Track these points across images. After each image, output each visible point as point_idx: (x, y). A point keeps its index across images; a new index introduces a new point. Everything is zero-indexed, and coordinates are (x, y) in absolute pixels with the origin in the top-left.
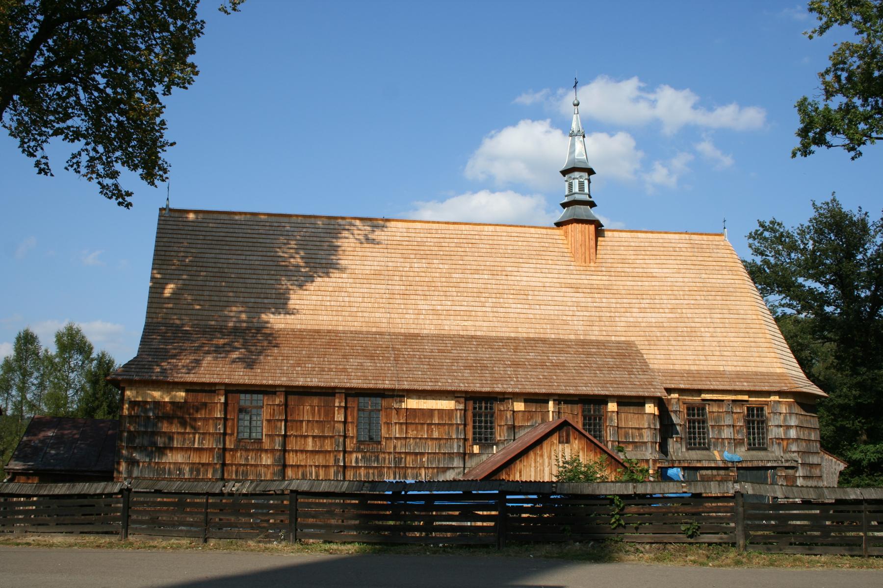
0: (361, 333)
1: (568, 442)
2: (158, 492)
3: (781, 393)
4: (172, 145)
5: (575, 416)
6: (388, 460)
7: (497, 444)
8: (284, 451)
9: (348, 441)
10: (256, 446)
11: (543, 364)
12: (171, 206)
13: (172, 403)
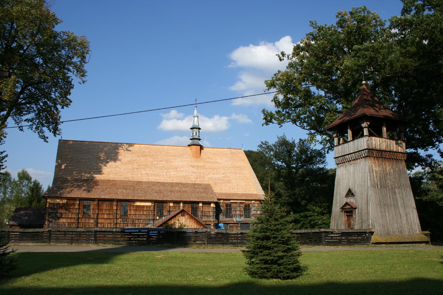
0: (123, 181)
1: (184, 216)
2: (59, 231)
3: (255, 200)
5: (188, 208)
6: (130, 221)
7: (164, 216)
8: (97, 218)
9: (117, 215)
10: (89, 217)
13: (63, 203)
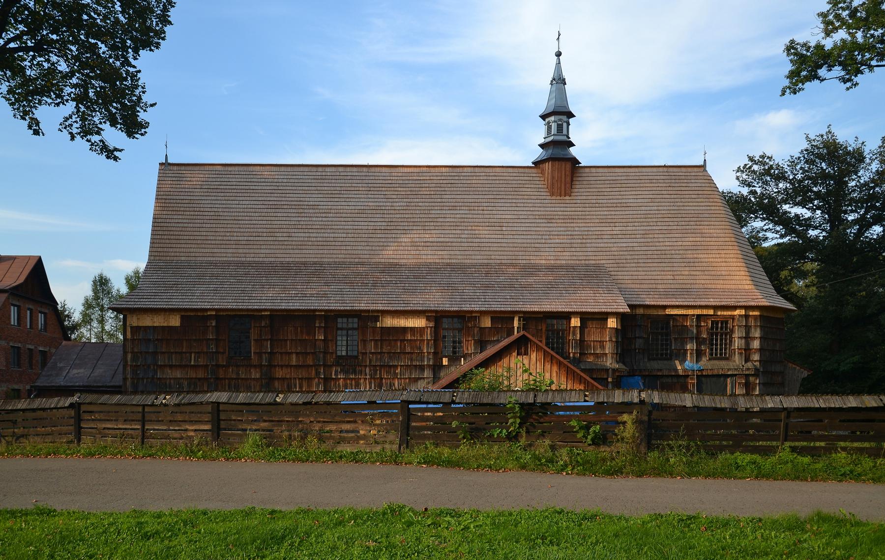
1: (526, 354)
4: (152, 105)
11: (512, 286)
12: (170, 161)
